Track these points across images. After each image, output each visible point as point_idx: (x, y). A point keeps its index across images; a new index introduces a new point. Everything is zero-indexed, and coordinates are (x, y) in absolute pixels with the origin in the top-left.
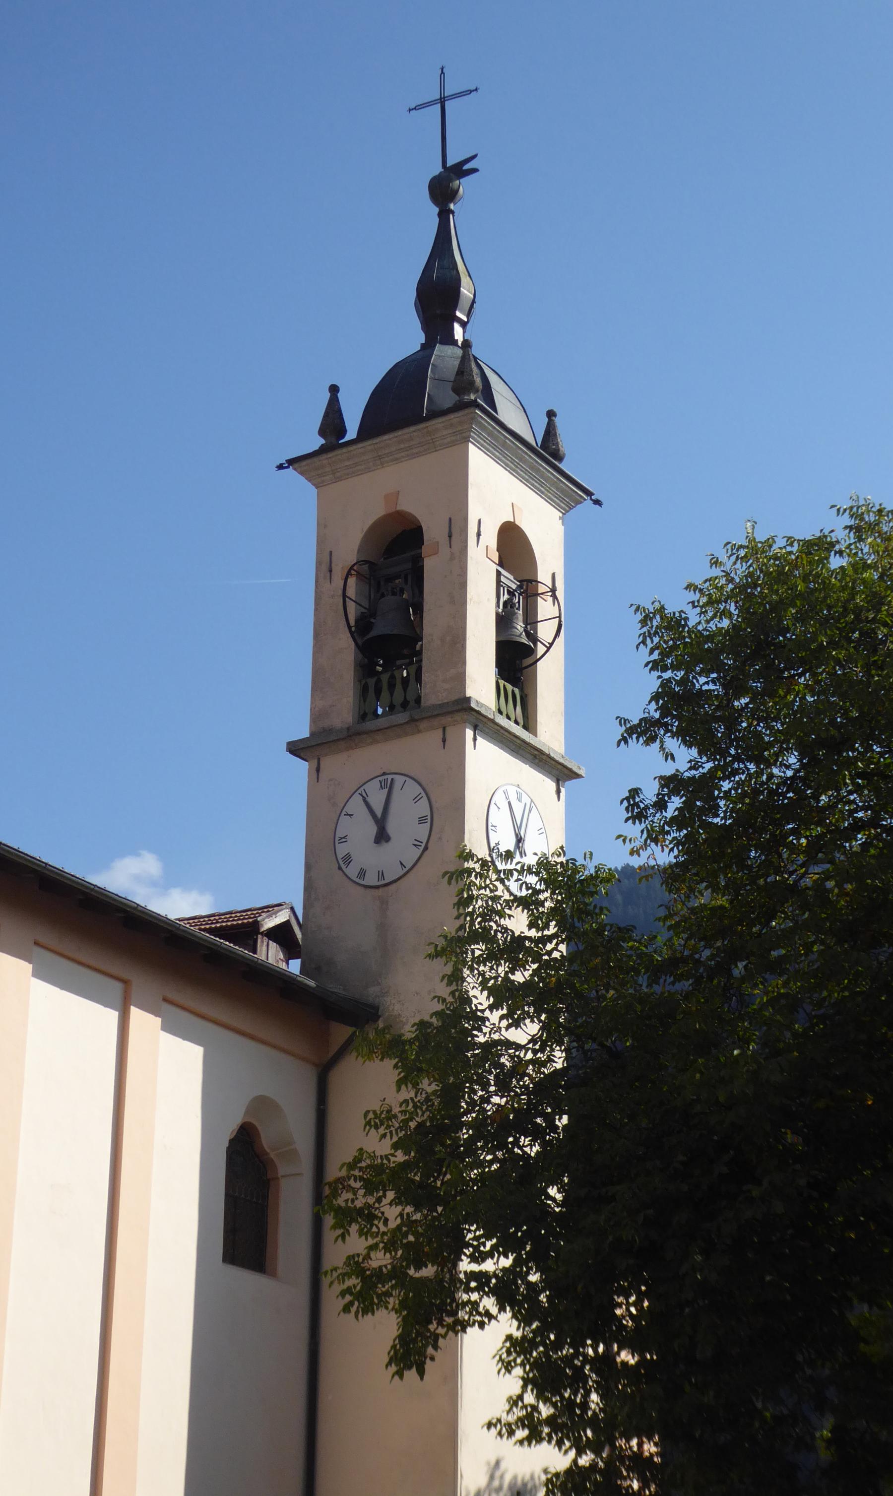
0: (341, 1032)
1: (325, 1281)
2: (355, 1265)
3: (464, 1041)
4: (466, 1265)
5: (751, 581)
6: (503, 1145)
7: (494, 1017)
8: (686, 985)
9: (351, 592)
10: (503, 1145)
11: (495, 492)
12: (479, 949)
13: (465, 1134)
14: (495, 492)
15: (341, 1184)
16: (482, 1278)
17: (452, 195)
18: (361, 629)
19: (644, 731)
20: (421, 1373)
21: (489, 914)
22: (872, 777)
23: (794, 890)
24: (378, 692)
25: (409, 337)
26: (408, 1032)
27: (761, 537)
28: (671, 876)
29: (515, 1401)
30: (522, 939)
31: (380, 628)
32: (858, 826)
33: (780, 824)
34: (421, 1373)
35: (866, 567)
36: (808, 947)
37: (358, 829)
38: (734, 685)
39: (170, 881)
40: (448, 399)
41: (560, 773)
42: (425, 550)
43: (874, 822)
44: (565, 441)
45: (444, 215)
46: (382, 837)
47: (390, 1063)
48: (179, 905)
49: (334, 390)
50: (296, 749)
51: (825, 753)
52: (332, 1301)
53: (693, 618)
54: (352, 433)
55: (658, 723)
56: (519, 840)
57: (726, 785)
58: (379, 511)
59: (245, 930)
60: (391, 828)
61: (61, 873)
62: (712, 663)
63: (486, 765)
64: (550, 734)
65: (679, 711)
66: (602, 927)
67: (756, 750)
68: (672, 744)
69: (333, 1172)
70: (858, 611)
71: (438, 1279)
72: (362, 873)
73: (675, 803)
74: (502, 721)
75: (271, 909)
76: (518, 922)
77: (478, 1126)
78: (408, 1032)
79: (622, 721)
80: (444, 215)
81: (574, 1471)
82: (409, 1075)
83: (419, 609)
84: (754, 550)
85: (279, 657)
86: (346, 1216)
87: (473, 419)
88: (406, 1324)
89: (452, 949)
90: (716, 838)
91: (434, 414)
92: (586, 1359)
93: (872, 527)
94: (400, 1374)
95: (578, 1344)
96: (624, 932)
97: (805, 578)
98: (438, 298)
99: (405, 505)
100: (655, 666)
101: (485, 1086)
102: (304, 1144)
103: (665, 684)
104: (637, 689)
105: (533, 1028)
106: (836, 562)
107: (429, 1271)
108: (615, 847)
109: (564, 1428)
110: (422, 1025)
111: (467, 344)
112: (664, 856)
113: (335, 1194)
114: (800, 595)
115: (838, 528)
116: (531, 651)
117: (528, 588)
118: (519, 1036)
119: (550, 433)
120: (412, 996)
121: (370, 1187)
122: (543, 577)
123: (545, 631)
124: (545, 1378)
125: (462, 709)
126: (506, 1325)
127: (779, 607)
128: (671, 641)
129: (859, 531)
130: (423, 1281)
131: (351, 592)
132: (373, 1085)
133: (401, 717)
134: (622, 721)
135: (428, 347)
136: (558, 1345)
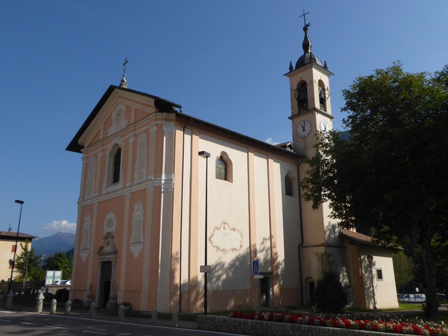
0: (300, 160)
1: (301, 197)
2: (306, 194)
3: (320, 159)
4: (322, 193)
5: (360, 84)
6: (327, 175)
7: (324, 156)
8: (354, 148)
9: (296, 93)
10: (327, 175)
11: (317, 75)
12: (321, 146)
13: (321, 174)
14: (317, 75)
15: (302, 182)
16: (325, 195)
17: (307, 29)
18: (298, 99)
19: (345, 109)
20: (317, 209)
21: (322, 140)
22: (382, 113)
23: (371, 132)
24: (301, 108)
25: (302, 53)
26: (311, 159)
27: (361, 77)
28: (350, 132)
29: (332, 212)
30: (327, 143)
31: (301, 98)
32: (381, 121)
33: (368, 122)
34: (317, 209)
35: (379, 79)
36: (374, 141)
37: (300, 129)
38: (359, 101)
39: (274, 141)
40: (309, 61)
41: (331, 118)
42: (307, 85)
43: (383, 120)
44: (328, 66)
45: (306, 33)
46: (304, 130)
47: (308, 164)
48: (274, 144)
49: (291, 62)
50: (289, 118)
51: (374, 109)
52: (303, 199)
53: (351, 91)
54: (294, 69)
55: (347, 108)
56: (325, 129)
57: (359, 117)
58: (299, 80)
59: (284, 146)
60: (305, 129)
61: (256, 140)
62: (355, 97)
63: (319, 117)
64: (329, 112)
65: (350, 106)
66: (340, 140)
67: (363, 111)
68: (349, 111)
69: (301, 181)
70: (378, 86)
71: (318, 195)
72: (301, 136)
73: (350, 120)
74: (321, 110)
75: (288, 143)
76: (327, 141)
77: (323, 172)
78: (311, 159)
79: (341, 108)
80: (306, 33)
81: (342, 222)
82: (312, 165)
83: (307, 95)
84: (360, 79)
85: (285, 104)
86: (304, 187)
87: (313, 64)
88: (314, 202)
89: (317, 146)
90: (356, 125)
91: (307, 64)
92: (343, 206)
93: (380, 73)
94: (314, 209)
95: (341, 203)
96: (344, 141)
97: (369, 82)
98: (306, 46)
99: (303, 79)
100: (346, 99)
101: (323, 166)
102: (296, 178)
103: (347, 101)
104: (343, 103)
105: (330, 157)
106: (374, 79)
107: (317, 194)
108: (342, 128)
109: (340, 216)
110: (313, 158)
111: (311, 52)
112: (349, 129)
113: (302, 184)
114: (369, 85)
115: (374, 73)
116: (325, 99)
117: (324, 89)
118: (328, 158)
119: (325, 65)
120: (311, 154)
121: (307, 182)
122: (326, 87)
123: (327, 96)
124: (336, 209)
125: (315, 109)
126: (330, 201)
127: (366, 87)
128: (348, 95)
129: (378, 74)
130: (316, 196)
131: (296, 93)
132: (306, 167)
133: (305, 112)
134: (341, 108)
135: (305, 54)
136: (338, 204)
